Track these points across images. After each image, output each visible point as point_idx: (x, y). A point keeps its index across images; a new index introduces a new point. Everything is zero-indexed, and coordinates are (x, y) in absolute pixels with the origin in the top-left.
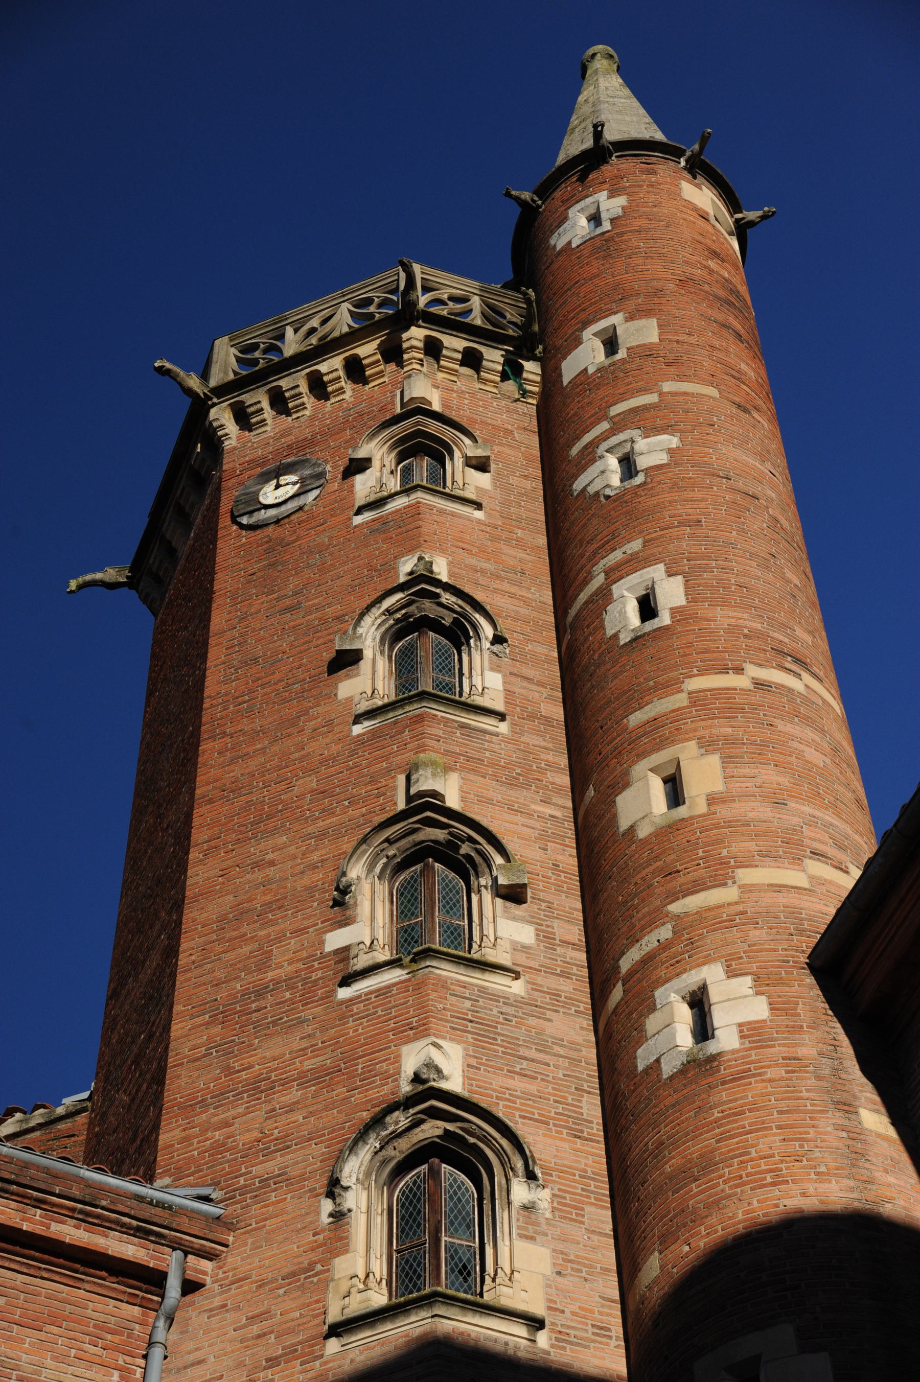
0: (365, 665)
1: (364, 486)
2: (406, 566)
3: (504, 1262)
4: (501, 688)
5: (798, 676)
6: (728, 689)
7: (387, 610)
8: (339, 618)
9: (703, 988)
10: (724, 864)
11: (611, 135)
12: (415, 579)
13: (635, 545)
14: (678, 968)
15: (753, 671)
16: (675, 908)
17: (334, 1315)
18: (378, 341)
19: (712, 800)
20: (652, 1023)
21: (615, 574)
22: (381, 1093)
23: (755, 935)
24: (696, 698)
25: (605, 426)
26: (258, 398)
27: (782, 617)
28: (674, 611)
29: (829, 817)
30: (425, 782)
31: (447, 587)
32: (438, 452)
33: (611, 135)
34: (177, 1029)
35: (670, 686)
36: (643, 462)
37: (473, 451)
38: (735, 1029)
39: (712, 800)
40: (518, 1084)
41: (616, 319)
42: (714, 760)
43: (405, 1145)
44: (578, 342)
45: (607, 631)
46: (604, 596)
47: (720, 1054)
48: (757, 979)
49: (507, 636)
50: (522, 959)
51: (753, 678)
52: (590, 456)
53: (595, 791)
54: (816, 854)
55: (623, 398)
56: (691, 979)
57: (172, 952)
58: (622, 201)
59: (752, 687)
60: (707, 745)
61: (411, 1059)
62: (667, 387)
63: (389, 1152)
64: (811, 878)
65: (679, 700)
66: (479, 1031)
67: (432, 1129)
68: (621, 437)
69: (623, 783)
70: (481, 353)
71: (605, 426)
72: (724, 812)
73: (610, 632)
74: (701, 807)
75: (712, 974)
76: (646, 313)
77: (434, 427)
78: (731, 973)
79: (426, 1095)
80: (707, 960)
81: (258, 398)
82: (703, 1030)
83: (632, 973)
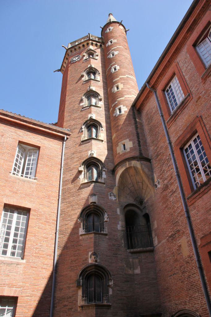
0: (84, 76)
1: (85, 58)
2: (89, 66)
3: (99, 135)
8: (82, 72)
9: (120, 108)
11: (111, 21)
12: (90, 67)
13: (114, 63)
14: (118, 106)
15: (126, 76)
17: (82, 140)
19: (122, 89)
20: (115, 111)
21: (112, 66)
22: (86, 119)
23: (127, 102)
26: (73, 49)
27: (130, 70)
28: (118, 70)
29: (134, 90)
30: (91, 88)
31: (93, 68)
32: (93, 55)
33: (112, 21)
34: (65, 114)
35: (118, 77)
36: (115, 54)
37: (96, 54)
39: (122, 89)
40: (101, 118)
41: (112, 40)
42: (122, 84)
43: (89, 124)
44: (108, 42)
45: (117, 152)
46: (111, 68)
47: (122, 114)
50: (101, 106)
52: (109, 54)
54: (133, 94)
55: (113, 48)
56: (116, 85)
57: (64, 106)
58: (113, 27)
60: (121, 83)
61: (89, 116)
62: (118, 46)
63: (87, 125)
64: (155, 236)
65: (119, 78)
66: (97, 113)
67: (92, 123)
68: (113, 52)
69: (112, 87)
72: (123, 90)
73: (112, 92)
74: (121, 89)
75: (121, 106)
76: (116, 39)
77: (92, 52)
78: (124, 106)
79: (91, 119)
80: (121, 105)
81: (73, 49)
82: (120, 112)
83: (113, 107)
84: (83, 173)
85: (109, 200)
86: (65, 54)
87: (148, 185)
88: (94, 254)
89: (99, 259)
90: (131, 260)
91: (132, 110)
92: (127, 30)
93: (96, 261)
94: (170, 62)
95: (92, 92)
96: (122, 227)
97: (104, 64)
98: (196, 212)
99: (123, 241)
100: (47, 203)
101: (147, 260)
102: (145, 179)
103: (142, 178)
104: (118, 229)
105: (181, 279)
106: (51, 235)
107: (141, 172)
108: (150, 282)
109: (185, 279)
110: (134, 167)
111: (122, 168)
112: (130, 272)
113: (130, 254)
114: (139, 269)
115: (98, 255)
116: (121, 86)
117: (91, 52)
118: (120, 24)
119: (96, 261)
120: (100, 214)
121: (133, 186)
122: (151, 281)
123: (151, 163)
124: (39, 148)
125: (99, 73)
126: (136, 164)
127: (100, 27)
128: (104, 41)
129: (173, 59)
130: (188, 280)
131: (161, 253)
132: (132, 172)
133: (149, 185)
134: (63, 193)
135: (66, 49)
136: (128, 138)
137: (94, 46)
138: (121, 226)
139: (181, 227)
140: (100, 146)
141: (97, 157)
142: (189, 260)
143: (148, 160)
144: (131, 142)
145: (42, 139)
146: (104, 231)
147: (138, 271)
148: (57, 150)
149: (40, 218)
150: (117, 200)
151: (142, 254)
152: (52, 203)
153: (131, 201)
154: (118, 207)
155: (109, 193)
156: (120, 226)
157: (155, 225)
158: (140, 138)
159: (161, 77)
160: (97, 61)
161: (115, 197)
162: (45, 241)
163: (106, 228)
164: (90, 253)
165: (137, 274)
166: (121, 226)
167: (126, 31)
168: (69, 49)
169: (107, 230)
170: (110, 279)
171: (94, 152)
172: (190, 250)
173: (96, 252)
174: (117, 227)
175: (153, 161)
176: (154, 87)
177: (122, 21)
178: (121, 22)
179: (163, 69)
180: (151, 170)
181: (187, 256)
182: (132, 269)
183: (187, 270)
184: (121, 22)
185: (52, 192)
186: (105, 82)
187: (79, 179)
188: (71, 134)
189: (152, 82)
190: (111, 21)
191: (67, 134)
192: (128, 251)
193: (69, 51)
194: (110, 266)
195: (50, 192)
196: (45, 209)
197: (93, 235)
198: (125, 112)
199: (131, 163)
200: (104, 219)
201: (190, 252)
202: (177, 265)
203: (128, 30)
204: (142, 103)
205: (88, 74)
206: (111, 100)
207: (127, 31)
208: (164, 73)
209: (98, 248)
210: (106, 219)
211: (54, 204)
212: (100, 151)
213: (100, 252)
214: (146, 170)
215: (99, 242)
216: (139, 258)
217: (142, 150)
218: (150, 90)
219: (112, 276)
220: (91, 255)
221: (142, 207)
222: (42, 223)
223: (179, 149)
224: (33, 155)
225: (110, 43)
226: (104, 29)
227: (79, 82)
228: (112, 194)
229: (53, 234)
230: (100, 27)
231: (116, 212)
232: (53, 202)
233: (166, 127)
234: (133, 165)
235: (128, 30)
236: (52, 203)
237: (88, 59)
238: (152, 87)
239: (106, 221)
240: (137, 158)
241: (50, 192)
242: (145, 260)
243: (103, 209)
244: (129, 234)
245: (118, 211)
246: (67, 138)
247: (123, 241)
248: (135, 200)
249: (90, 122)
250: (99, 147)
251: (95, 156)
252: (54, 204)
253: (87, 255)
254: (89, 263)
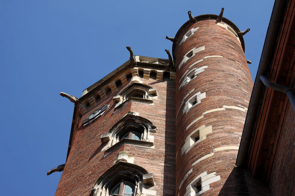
4: (153, 139)
5: (244, 108)
6: (217, 111)
7: (119, 128)
10: (209, 148)
11: (193, 16)
16: (193, 165)
18: (125, 74)
24: (205, 116)
25: (188, 70)
26: (93, 98)
38: (209, 185)
48: (217, 172)
49: (155, 125)
51: (226, 108)
53: (193, 170)
59: (225, 110)
70: (157, 71)
71: (188, 70)
81: (93, 98)
118: (220, 18)
125: (153, 127)
127: (167, 38)
135: (72, 100)
137: (147, 77)
160: (153, 104)
177: (223, 9)
178: (222, 14)
184: (222, 14)
186: (169, 145)
189: (277, 68)
190: (193, 16)
193: (82, 106)
198: (213, 185)
203: (247, 31)
205: (122, 135)
225: (186, 59)
226: (176, 41)
227: (95, 157)
230: (167, 38)
235: (247, 31)
237: (126, 104)
238: (278, 82)
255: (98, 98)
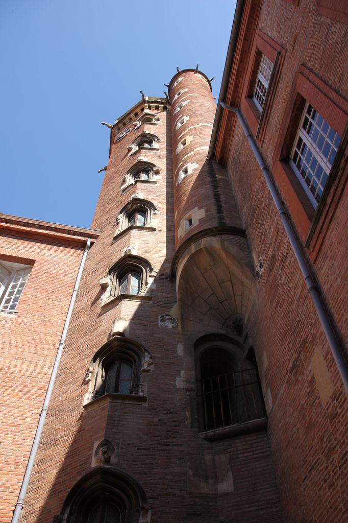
21: (177, 122)
24: (189, 130)
26: (121, 125)
67: (135, 206)
72: (192, 143)
81: (121, 125)
84: (109, 289)
85: (157, 328)
86: (111, 137)
87: (242, 282)
88: (106, 443)
89: (115, 456)
90: (208, 458)
91: (208, 164)
92: (210, 79)
93: (107, 461)
94: (248, 40)
95: (142, 165)
96: (188, 381)
97: (169, 128)
98: (330, 264)
99: (187, 413)
100: (32, 355)
101: (251, 453)
102: (235, 269)
103: (228, 268)
104: (174, 386)
105: (327, 477)
106: (29, 420)
107: (224, 255)
108: (262, 512)
109: (336, 473)
110: (206, 248)
111: (184, 258)
112: (205, 488)
113: (207, 444)
114: (231, 480)
115: (116, 448)
116: (189, 139)
117: (148, 118)
119: (107, 461)
120: (134, 359)
121: (214, 293)
122: (262, 509)
123: (246, 237)
124: (31, 262)
125: (158, 140)
126: (214, 242)
127: (165, 85)
128: (168, 104)
129: (252, 31)
130: (342, 472)
131: (280, 426)
132: (205, 260)
133: (245, 280)
134: (71, 335)
135: (109, 127)
136: (196, 205)
138: (184, 381)
139: (307, 329)
140: (146, 238)
141: (141, 256)
142: (336, 409)
143: (240, 233)
144: (203, 211)
145: (41, 248)
146: (138, 391)
147: (226, 486)
148: (69, 263)
149: (10, 384)
150: (180, 328)
151: (238, 441)
152: (42, 355)
153: (214, 327)
154: (181, 342)
155: (160, 316)
156: (183, 379)
157: (265, 362)
158: (223, 201)
159: (241, 78)
161: (174, 323)
162: (11, 431)
163: (146, 384)
164: (96, 445)
165: (225, 495)
166: (184, 381)
167: (209, 82)
168: (115, 126)
169: (146, 390)
170: (143, 508)
171: (134, 248)
172: (333, 378)
173: (110, 440)
174: (174, 383)
175: (252, 233)
176: (234, 104)
178: (197, 68)
179: (240, 60)
180: (247, 249)
181: (331, 398)
182: (210, 481)
183: (336, 439)
184: (197, 68)
185: (46, 334)
187: (101, 300)
188: (100, 234)
189: (229, 97)
190: (180, 71)
191: (91, 236)
192: (202, 435)
193: (115, 130)
194: (145, 474)
195: (42, 336)
196: (23, 367)
197: (109, 400)
198: (195, 170)
199: (200, 244)
200: (140, 364)
201: (335, 381)
202: (313, 440)
203: (213, 79)
204: (222, 147)
206: (174, 161)
207: (211, 80)
208: (245, 68)
209: (118, 431)
210: (145, 367)
211: (47, 356)
212: (149, 245)
213: (121, 440)
214: (234, 250)
215: (122, 417)
216: (228, 451)
217: (226, 218)
218: (230, 112)
219: (151, 501)
220: (98, 447)
221: (241, 340)
222: (11, 395)
223: (279, 162)
224: (23, 277)
228: (166, 317)
229: (33, 415)
231: (175, 351)
232: (47, 352)
233: (255, 145)
234: (204, 245)
235: (213, 79)
236: (42, 355)
239: (144, 371)
240: (212, 232)
241: (42, 336)
242: (245, 455)
243: (139, 346)
244: (204, 396)
245: (180, 350)
246: (92, 243)
247: (187, 413)
248: (223, 325)
249: (132, 206)
250: (145, 240)
251: (134, 252)
252: (47, 356)
253: (90, 449)
254: (90, 467)
255: (124, 124)
